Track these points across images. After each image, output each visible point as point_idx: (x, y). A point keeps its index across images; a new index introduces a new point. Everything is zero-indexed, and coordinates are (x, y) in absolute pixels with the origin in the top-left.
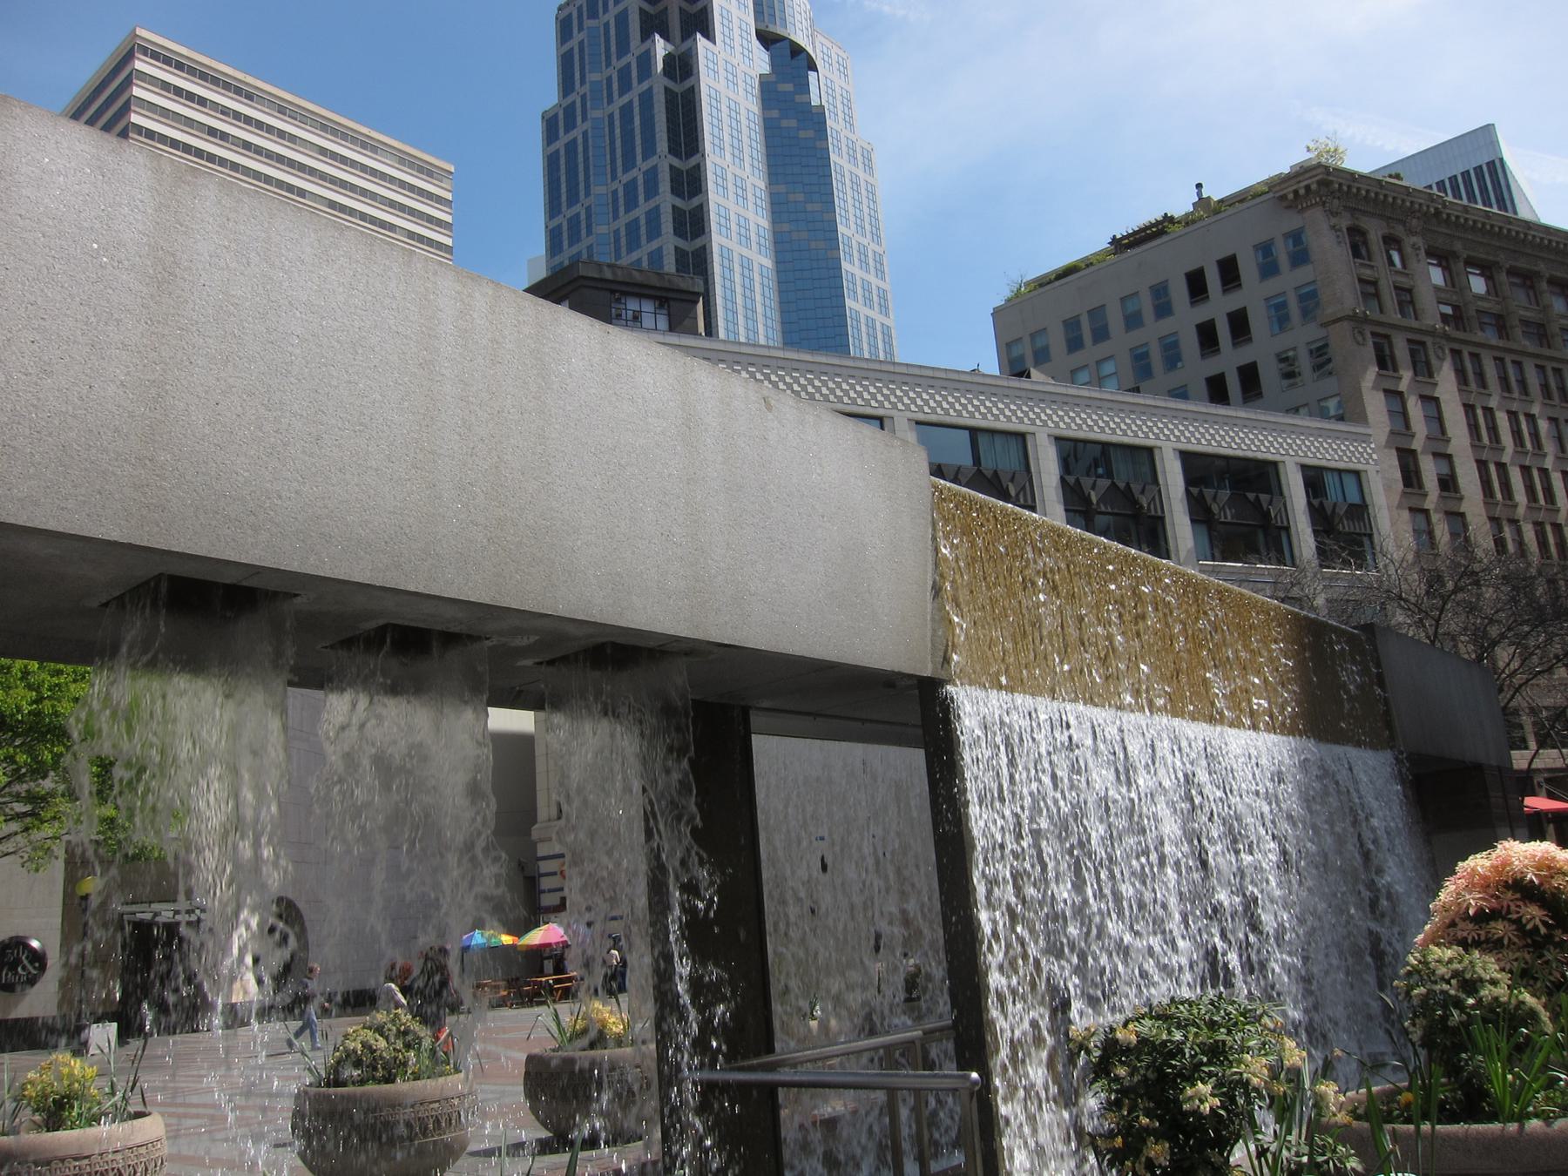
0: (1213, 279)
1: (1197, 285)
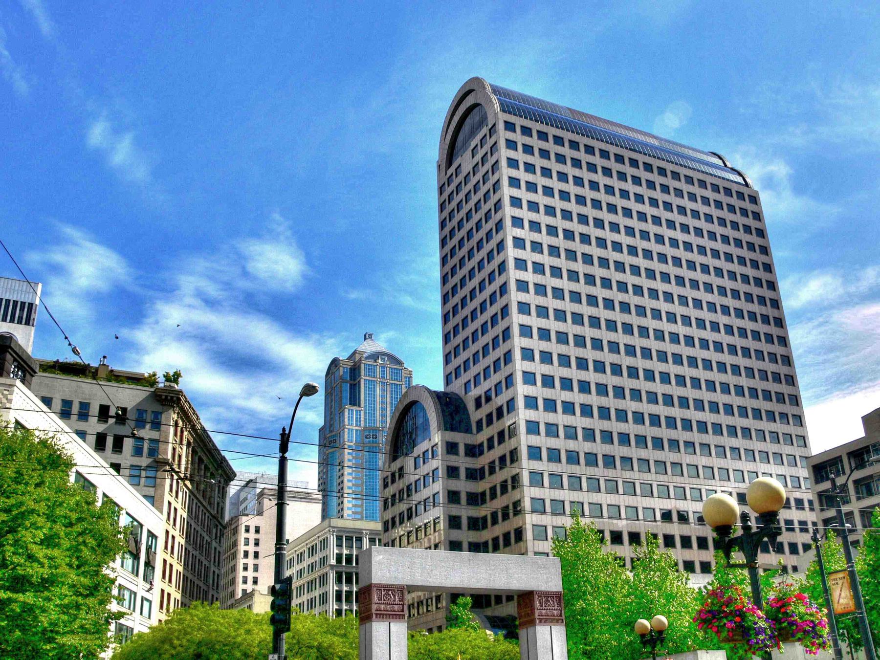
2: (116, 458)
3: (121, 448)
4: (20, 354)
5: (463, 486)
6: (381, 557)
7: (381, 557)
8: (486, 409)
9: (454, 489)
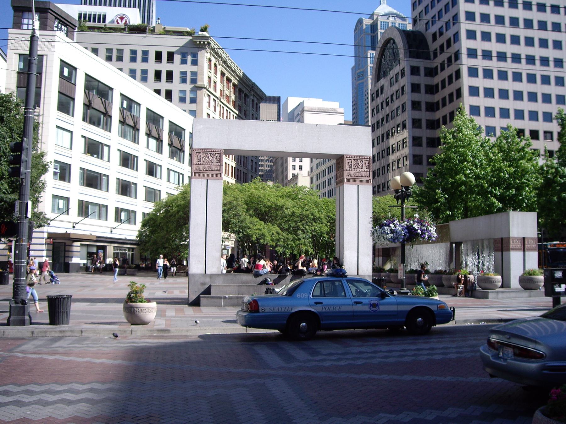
0: (139, 56)
1: (158, 56)
2: (169, 86)
3: (160, 79)
4: (59, 14)
5: (423, 97)
6: (202, 126)
7: (202, 126)
8: (441, 40)
9: (417, 100)
